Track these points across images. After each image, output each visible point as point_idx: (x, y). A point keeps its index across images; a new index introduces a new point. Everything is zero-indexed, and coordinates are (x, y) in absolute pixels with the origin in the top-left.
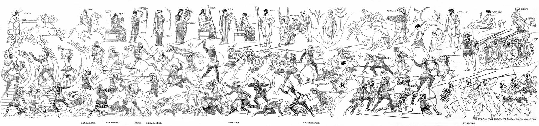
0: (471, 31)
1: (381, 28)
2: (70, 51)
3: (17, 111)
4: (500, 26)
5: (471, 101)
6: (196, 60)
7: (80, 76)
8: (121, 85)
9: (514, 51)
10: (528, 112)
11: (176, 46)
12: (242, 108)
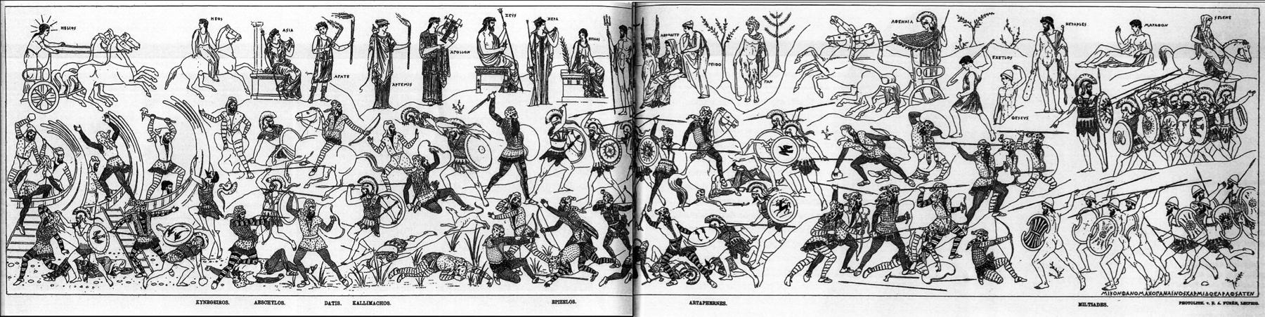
0: (1094, 72)
1: (876, 64)
2: (168, 121)
3: (46, 270)
4: (1164, 62)
5: (1097, 248)
6: (472, 145)
7: (193, 184)
8: (289, 209)
9: (1199, 123)
10: (1233, 276)
11: (423, 109)
12: (582, 267)
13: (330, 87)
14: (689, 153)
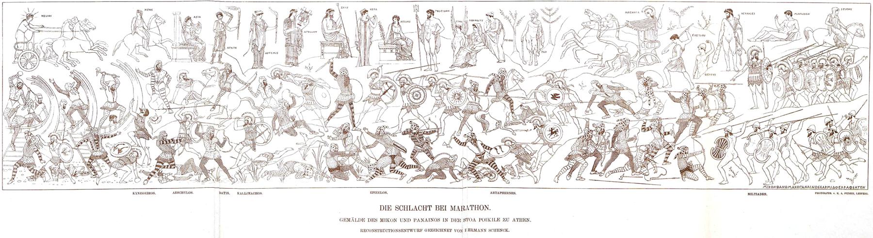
0: (759, 45)
2: (115, 77)
6: (318, 92)
7: (131, 117)
9: (830, 77)
12: (392, 170)
13: (224, 55)
14: (490, 98)
